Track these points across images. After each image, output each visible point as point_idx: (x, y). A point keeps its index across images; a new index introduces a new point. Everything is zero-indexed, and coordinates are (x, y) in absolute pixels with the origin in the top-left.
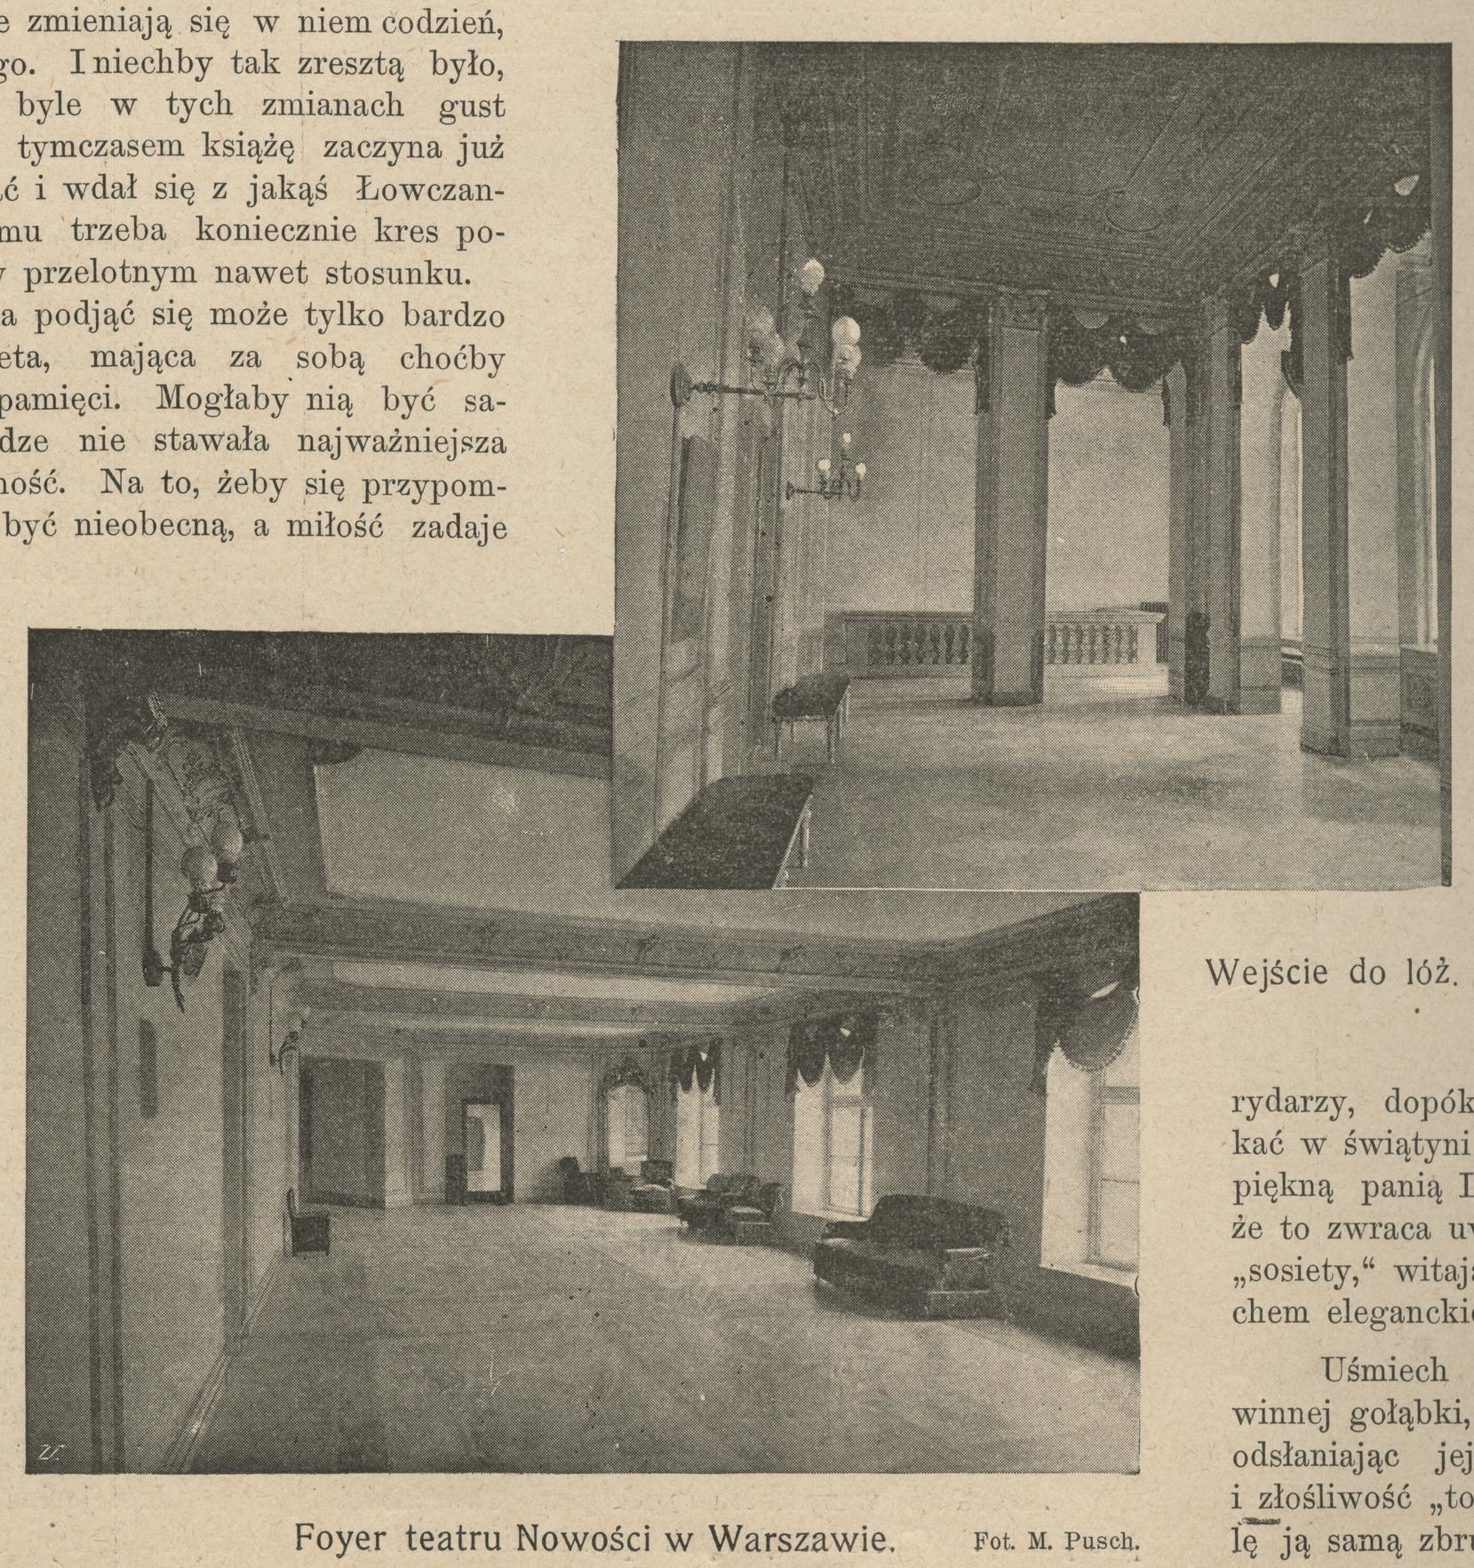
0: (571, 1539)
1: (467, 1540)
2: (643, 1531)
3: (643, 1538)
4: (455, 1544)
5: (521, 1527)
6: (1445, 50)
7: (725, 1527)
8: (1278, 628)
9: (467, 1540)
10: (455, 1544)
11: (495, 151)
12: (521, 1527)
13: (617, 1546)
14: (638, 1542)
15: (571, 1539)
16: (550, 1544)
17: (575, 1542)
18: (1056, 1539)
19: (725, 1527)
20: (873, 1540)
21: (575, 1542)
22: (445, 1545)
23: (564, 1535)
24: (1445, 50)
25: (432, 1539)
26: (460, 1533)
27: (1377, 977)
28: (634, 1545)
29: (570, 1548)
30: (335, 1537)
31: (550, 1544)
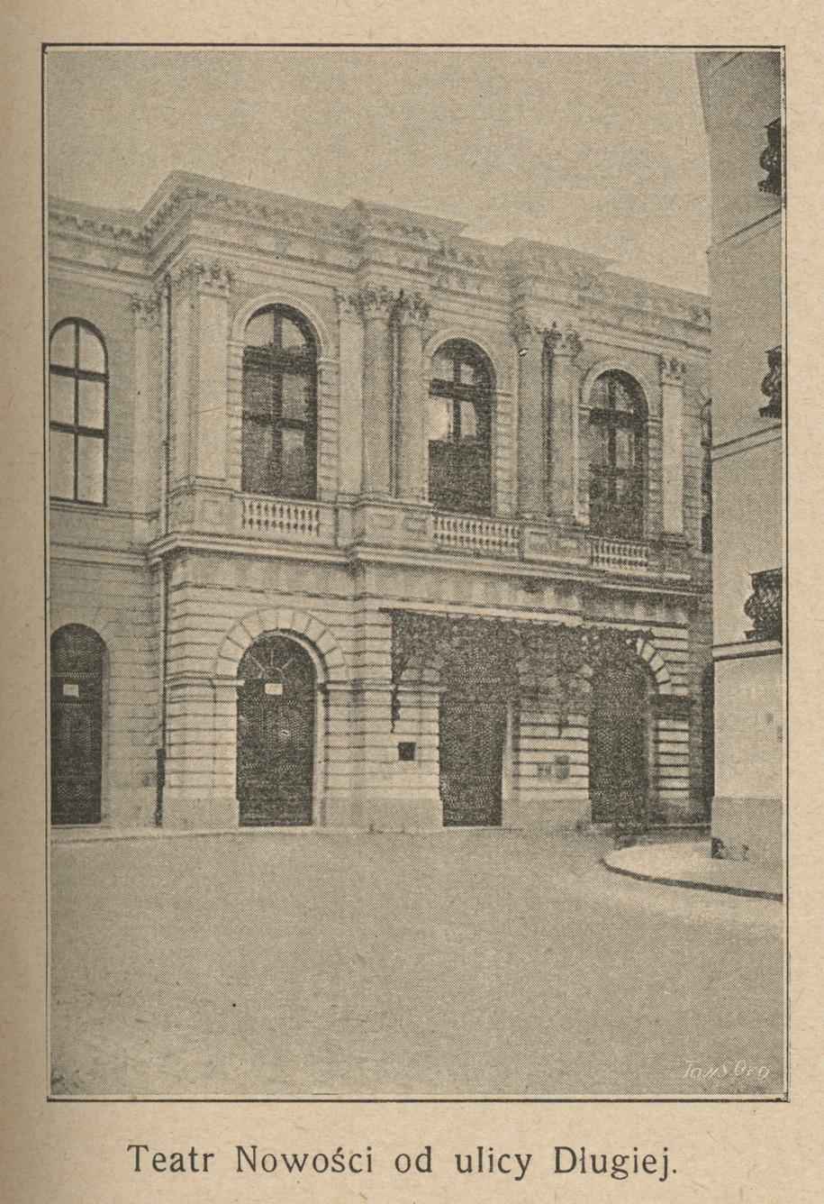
0: (291, 1160)
1: (199, 1161)
2: (364, 1153)
3: (365, 1160)
4: (187, 1164)
5: (240, 1148)
6: (772, 60)
7: (295, 1156)
8: (651, 660)
9: (199, 1161)
10: (187, 1164)
11: (277, 783)
12: (240, 1148)
13: (338, 1168)
14: (360, 1163)
15: (291, 1160)
16: (269, 1166)
17: (297, 1164)
18: (666, 1153)
19: (295, 1156)
20: (644, 1164)
21: (297, 1164)
22: (177, 1166)
23: (284, 1156)
24: (772, 60)
25: (164, 1160)
26: (192, 1154)
27: (403, 1161)
28: (357, 1167)
29: (290, 1169)
30: (279, 1158)
31: (269, 1166)
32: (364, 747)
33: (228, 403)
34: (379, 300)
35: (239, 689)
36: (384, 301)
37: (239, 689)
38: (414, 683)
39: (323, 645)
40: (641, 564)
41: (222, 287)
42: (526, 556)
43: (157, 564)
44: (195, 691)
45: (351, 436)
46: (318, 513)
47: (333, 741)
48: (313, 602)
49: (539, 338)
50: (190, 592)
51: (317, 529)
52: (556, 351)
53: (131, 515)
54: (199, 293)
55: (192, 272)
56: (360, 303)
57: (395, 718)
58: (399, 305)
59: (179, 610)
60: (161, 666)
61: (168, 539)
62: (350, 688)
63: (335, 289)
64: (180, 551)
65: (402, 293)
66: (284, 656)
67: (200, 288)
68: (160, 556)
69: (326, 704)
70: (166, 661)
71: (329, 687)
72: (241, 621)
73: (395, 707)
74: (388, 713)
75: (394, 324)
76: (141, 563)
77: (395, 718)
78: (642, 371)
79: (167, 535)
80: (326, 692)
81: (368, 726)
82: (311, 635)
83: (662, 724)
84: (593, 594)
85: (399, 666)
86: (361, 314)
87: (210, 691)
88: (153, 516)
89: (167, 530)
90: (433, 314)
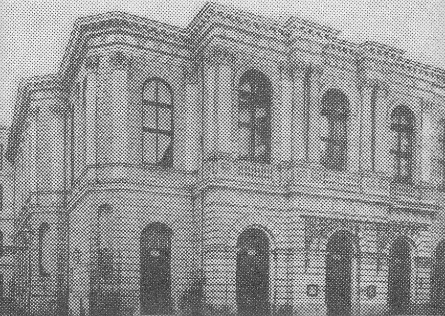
32: (292, 286)
33: (90, 251)
34: (382, 88)
35: (238, 253)
36: (303, 69)
37: (238, 253)
38: (316, 250)
39: (275, 233)
40: (412, 196)
41: (229, 61)
42: (364, 191)
43: (198, 194)
44: (219, 253)
45: (286, 123)
46: (272, 170)
47: (278, 289)
48: (270, 213)
49: (371, 88)
50: (216, 207)
51: (272, 178)
52: (377, 95)
53: (185, 172)
54: (218, 64)
55: (217, 52)
56: (291, 72)
57: (307, 266)
58: (376, 87)
59: (208, 216)
60: (200, 242)
61: (203, 183)
62: (286, 252)
63: (280, 63)
64: (211, 187)
65: (311, 65)
66: (255, 238)
67: (219, 61)
68: (199, 190)
69: (275, 259)
70: (202, 240)
71: (277, 252)
72: (238, 221)
73: (307, 261)
74: (302, 264)
75: (307, 81)
76: (189, 194)
77: (307, 266)
78: (414, 105)
79: (203, 180)
80: (275, 254)
81: (295, 270)
82: (269, 228)
83: (420, 269)
84: (390, 209)
85: (308, 242)
86: (292, 76)
87: (225, 254)
88: (195, 173)
89: (203, 178)
90: (324, 76)
